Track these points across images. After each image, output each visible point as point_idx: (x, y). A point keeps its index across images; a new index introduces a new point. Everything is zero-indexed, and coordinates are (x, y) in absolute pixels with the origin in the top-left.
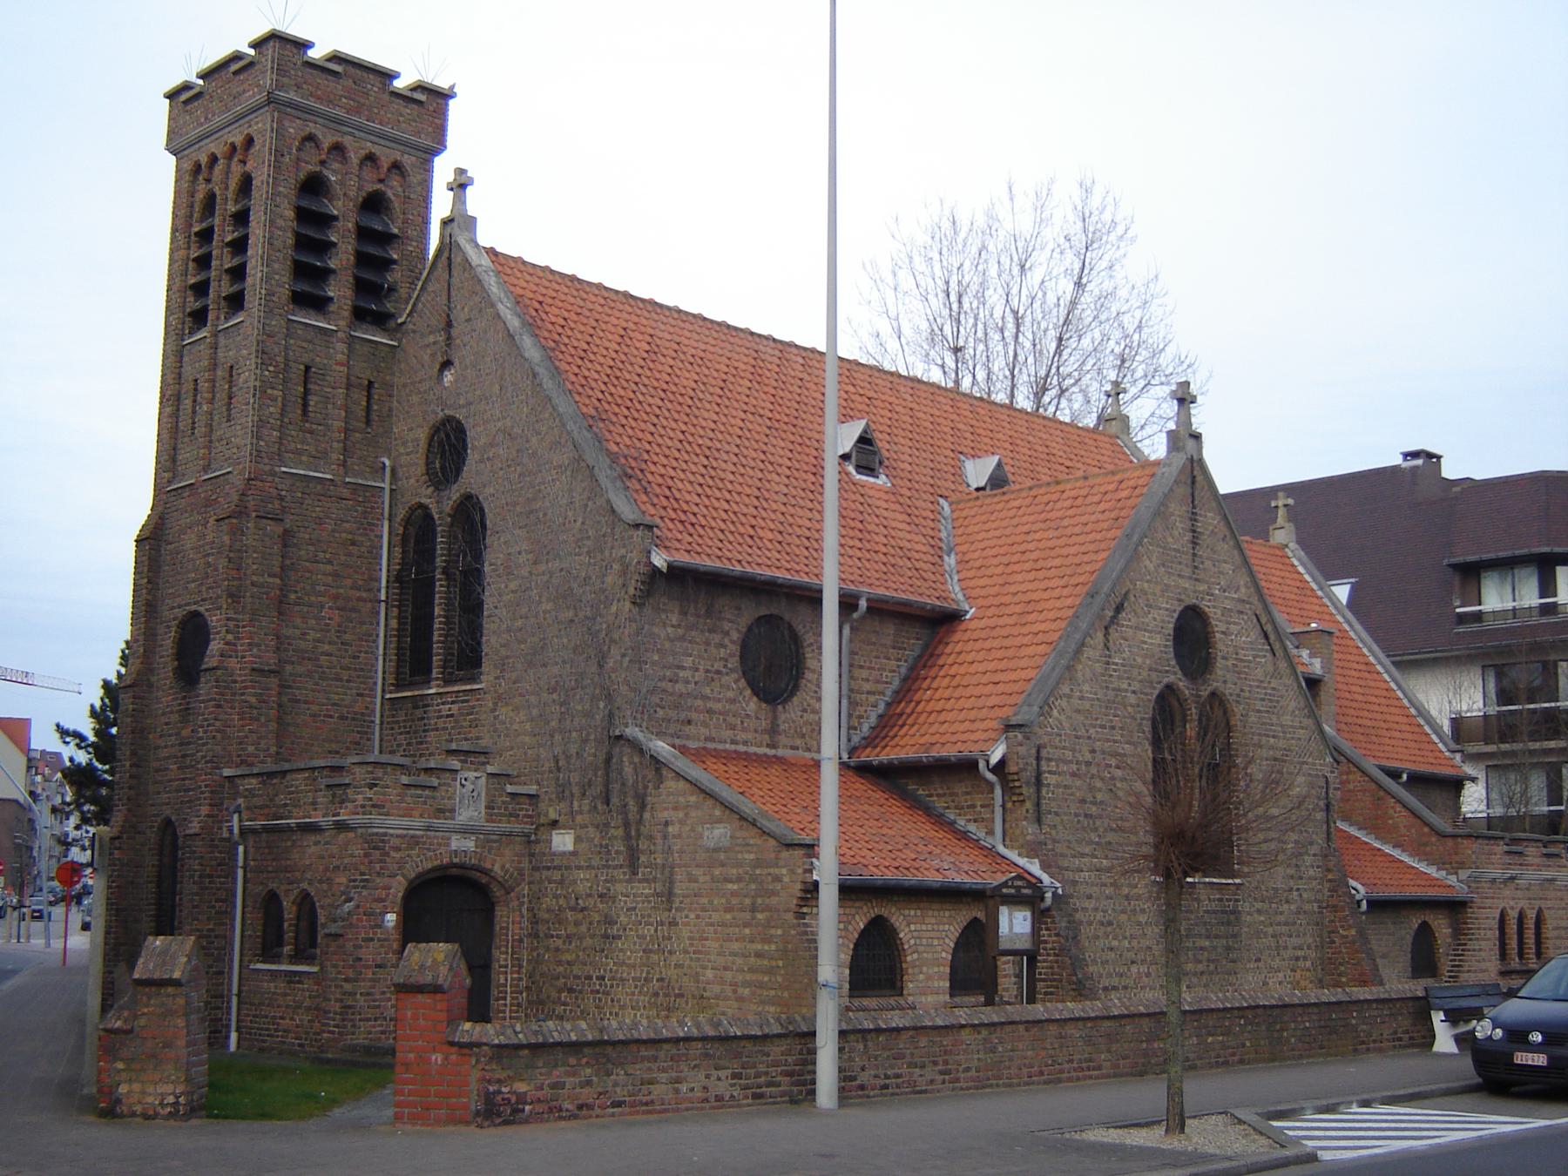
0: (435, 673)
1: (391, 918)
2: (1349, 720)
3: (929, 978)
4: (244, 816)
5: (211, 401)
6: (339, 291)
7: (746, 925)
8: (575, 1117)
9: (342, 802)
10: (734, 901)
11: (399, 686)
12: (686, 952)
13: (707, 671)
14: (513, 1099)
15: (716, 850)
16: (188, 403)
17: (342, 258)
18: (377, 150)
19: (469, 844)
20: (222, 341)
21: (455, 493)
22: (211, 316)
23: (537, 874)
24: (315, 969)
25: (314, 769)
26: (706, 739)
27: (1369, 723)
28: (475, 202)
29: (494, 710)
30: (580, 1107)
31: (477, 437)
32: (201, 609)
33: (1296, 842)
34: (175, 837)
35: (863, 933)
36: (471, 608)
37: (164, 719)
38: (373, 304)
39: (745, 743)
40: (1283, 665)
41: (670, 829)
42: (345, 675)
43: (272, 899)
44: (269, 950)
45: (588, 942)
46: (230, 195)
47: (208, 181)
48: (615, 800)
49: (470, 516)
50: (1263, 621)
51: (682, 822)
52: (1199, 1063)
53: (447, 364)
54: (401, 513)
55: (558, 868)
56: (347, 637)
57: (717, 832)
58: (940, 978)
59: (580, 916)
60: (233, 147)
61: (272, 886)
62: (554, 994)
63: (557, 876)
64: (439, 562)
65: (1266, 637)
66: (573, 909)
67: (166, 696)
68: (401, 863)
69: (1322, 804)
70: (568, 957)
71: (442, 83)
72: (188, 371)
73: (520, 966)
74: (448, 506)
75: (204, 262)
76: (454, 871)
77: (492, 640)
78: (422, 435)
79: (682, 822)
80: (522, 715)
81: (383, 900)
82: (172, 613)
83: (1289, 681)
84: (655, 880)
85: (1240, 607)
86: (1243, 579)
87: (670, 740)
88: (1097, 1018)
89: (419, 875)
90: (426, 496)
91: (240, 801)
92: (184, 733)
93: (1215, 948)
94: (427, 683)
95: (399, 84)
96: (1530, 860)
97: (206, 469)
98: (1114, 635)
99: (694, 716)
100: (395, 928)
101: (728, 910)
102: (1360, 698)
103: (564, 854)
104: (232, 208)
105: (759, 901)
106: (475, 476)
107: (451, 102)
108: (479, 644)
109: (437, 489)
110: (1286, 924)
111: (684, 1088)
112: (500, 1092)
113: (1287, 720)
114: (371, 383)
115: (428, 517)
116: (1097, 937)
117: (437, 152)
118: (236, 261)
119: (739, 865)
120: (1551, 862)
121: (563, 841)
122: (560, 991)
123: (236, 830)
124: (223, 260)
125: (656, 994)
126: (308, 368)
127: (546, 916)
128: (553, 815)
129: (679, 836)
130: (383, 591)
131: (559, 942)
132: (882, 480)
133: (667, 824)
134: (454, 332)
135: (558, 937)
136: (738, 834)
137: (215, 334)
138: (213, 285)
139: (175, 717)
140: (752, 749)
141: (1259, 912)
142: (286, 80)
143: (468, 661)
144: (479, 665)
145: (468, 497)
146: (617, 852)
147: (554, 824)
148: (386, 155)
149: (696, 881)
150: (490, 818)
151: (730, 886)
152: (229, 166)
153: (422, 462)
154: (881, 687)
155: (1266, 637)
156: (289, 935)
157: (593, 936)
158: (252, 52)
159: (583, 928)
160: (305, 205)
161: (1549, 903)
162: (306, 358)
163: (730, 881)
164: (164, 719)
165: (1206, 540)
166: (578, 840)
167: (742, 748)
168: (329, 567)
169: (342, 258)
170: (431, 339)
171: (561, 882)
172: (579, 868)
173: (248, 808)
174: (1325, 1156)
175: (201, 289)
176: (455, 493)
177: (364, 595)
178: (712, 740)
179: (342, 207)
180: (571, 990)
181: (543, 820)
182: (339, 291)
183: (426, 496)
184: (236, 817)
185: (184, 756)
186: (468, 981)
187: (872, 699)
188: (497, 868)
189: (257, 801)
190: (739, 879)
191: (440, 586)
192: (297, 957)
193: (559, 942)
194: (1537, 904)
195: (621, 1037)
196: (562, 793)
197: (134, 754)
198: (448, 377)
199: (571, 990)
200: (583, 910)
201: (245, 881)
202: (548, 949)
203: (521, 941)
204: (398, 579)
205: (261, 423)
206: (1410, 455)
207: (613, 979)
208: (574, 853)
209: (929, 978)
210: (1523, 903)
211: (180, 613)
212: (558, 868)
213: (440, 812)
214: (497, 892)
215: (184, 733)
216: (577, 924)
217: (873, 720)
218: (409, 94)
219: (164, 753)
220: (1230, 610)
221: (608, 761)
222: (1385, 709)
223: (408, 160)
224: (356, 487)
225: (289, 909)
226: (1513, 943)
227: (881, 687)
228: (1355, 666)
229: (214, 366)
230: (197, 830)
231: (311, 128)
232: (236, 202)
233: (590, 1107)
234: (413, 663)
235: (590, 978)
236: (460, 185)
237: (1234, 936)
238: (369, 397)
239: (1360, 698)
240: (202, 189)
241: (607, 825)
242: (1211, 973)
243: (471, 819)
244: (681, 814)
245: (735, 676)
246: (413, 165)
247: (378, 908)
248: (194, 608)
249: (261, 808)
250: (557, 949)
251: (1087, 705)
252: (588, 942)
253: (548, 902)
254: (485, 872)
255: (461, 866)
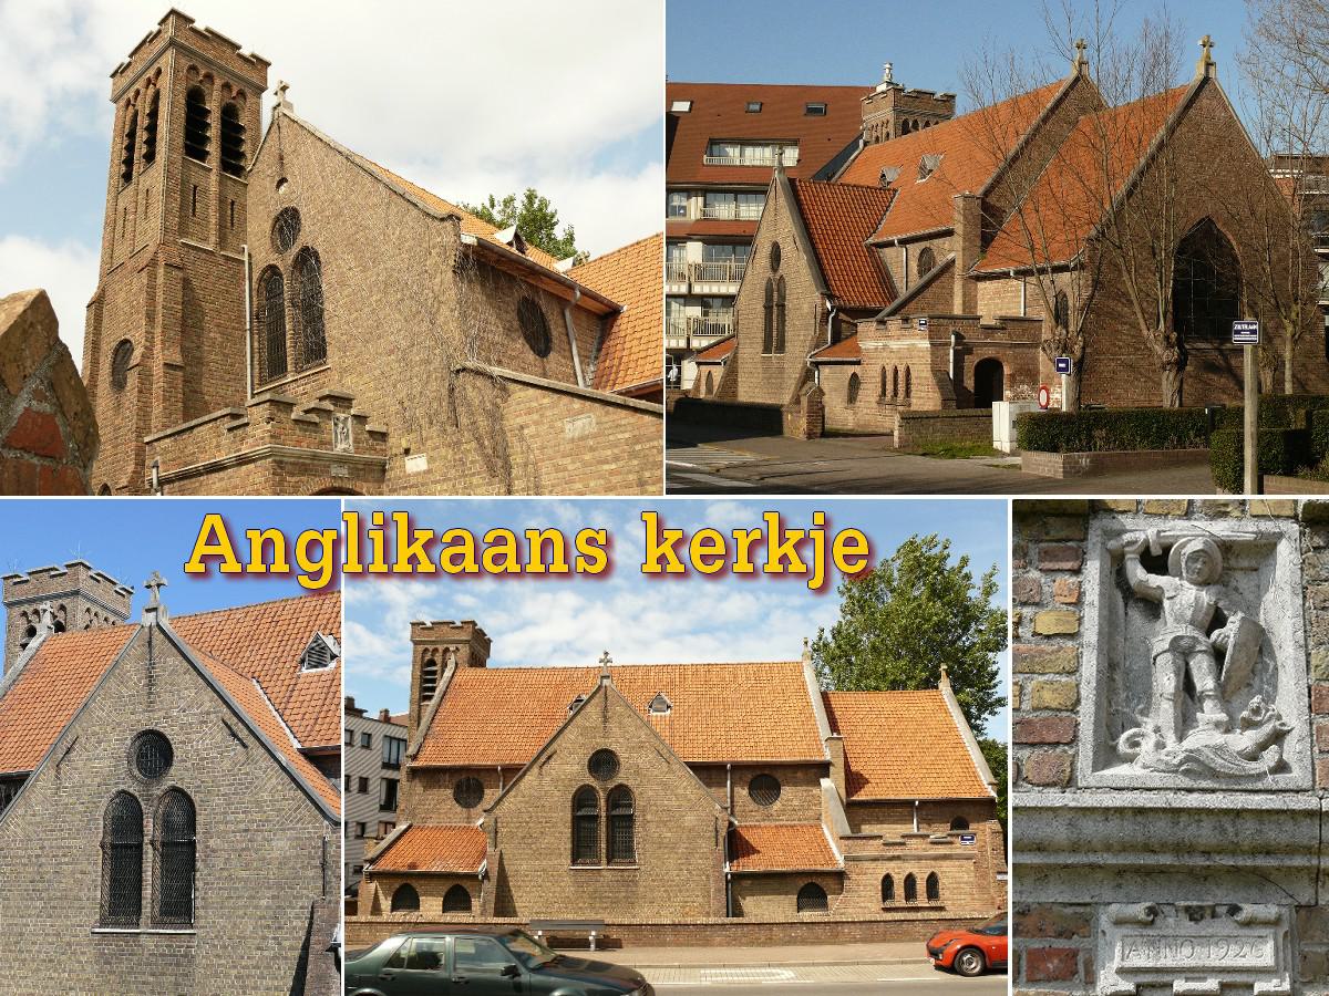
4: (160, 469)
6: (213, 148)
10: (614, 480)
15: (582, 438)
17: (214, 131)
18: (231, 82)
25: (215, 419)
38: (232, 161)
41: (526, 431)
47: (134, 105)
48: (464, 420)
53: (282, 181)
54: (256, 276)
57: (579, 423)
77: (333, 330)
78: (267, 226)
79: (536, 423)
80: (366, 378)
90: (274, 259)
103: (418, 474)
105: (647, 474)
106: (309, 234)
107: (269, 69)
123: (155, 481)
128: (405, 445)
129: (538, 435)
130: (248, 324)
133: (522, 428)
136: (605, 419)
145: (305, 249)
146: (472, 462)
149: (565, 470)
151: (606, 467)
153: (269, 241)
163: (606, 462)
166: (431, 460)
169: (214, 131)
173: (164, 462)
176: (295, 250)
179: (213, 105)
182: (213, 148)
184: (154, 470)
185: (117, 438)
190: (616, 459)
196: (410, 426)
198: (283, 189)
205: (167, 212)
208: (429, 471)
213: (322, 443)
221: (452, 390)
224: (227, 258)
230: (126, 484)
231: (23, 608)
243: (345, 450)
244: (535, 417)
249: (174, 460)
251: (38, 819)
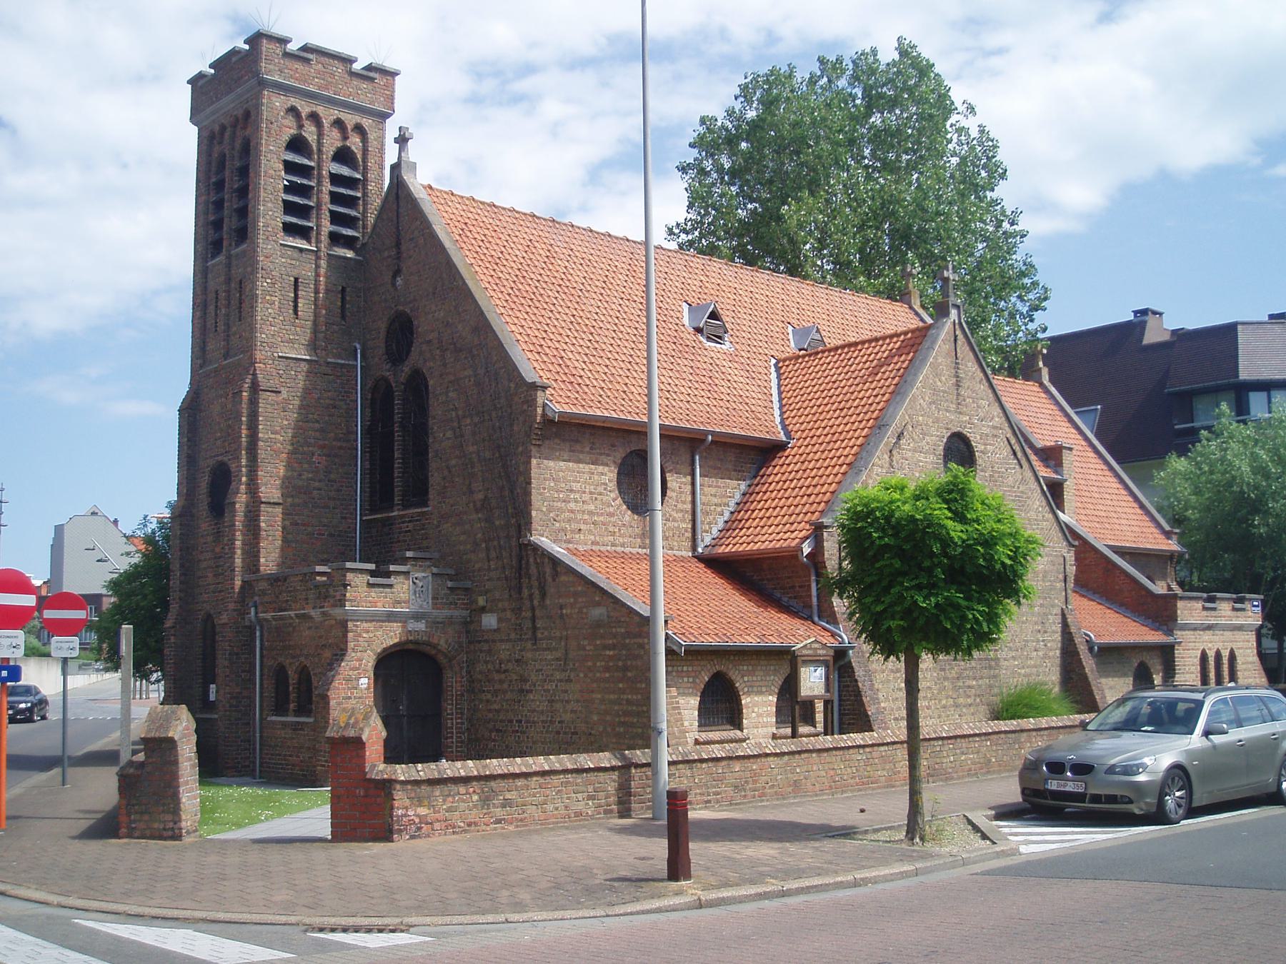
0: (397, 500)
1: (364, 682)
2: (1088, 512)
3: (759, 715)
5: (228, 306)
7: (620, 681)
8: (466, 831)
9: (326, 597)
11: (373, 511)
12: (578, 701)
13: (591, 493)
14: (417, 820)
16: (212, 308)
18: (343, 116)
19: (421, 626)
20: (234, 262)
21: (406, 369)
22: (225, 243)
23: (472, 647)
24: (311, 720)
26: (593, 543)
27: (1103, 514)
28: (414, 152)
29: (438, 526)
30: (469, 825)
31: (423, 326)
32: (226, 459)
33: (1041, 605)
34: (214, 626)
35: (708, 685)
36: (419, 451)
37: (202, 541)
39: (623, 545)
40: (1029, 474)
42: (331, 504)
43: (281, 673)
44: (280, 709)
45: (509, 695)
46: (236, 154)
49: (418, 385)
50: (1013, 441)
51: (572, 606)
52: (955, 775)
53: (397, 272)
55: (486, 641)
56: (332, 476)
58: (768, 715)
59: (503, 676)
60: (237, 120)
61: (281, 659)
62: (487, 734)
63: (486, 647)
64: (397, 418)
65: (1015, 453)
66: (498, 672)
67: (205, 526)
68: (369, 642)
69: (1061, 576)
70: (496, 706)
71: (390, 64)
72: (212, 285)
73: (462, 714)
74: (403, 377)
75: (219, 205)
76: (411, 647)
78: (383, 326)
81: (358, 669)
82: (206, 464)
83: (1034, 486)
84: (556, 649)
85: (995, 432)
86: (996, 410)
87: (564, 545)
88: (873, 745)
89: (385, 650)
90: (385, 371)
91: (256, 598)
92: (217, 550)
93: (980, 686)
94: (391, 508)
95: (357, 67)
96: (1223, 613)
97: (226, 356)
98: (896, 457)
99: (583, 527)
100: (368, 689)
101: (607, 669)
102: (1097, 495)
104: (238, 164)
108: (427, 478)
109: (394, 364)
110: (1035, 666)
111: (550, 807)
112: (406, 815)
113: (1032, 515)
114: (343, 290)
115: (389, 386)
116: (889, 681)
117: (389, 115)
118: (241, 204)
119: (615, 636)
120: (1239, 613)
121: (490, 621)
122: (491, 731)
124: (231, 204)
125: (558, 733)
126: (296, 280)
127: (480, 677)
131: (489, 696)
132: (726, 346)
134: (403, 248)
135: (488, 692)
137: (229, 257)
138: (226, 220)
139: (210, 539)
140: (627, 550)
141: (1014, 658)
142: (271, 67)
143: (418, 492)
144: (427, 492)
147: (483, 610)
148: (350, 119)
150: (435, 606)
152: (234, 133)
153: (383, 345)
154: (725, 500)
155: (1015, 453)
156: (293, 696)
157: (512, 691)
158: (247, 47)
159: (505, 686)
160: (278, 156)
161: (1240, 645)
162: (295, 273)
164: (202, 541)
165: (965, 383)
166: (500, 620)
167: (619, 549)
168: (317, 425)
170: (386, 254)
171: (489, 651)
172: (502, 641)
174: (1023, 849)
175: (218, 225)
176: (406, 369)
177: (344, 445)
178: (598, 544)
180: (498, 731)
181: (474, 607)
183: (385, 371)
186: (384, 734)
187: (719, 509)
188: (442, 642)
189: (266, 599)
191: (397, 436)
192: (298, 712)
193: (489, 696)
194: (1229, 645)
195: (500, 772)
197: (182, 566)
199: (498, 731)
200: (505, 671)
201: (262, 656)
202: (481, 701)
203: (462, 695)
204: (367, 432)
206: (1136, 312)
207: (527, 722)
209: (759, 715)
210: (1220, 645)
211: (211, 462)
212: (486, 641)
214: (442, 660)
215: (217, 550)
216: (501, 682)
217: (721, 525)
218: (365, 73)
219: (204, 565)
220: (987, 435)
222: (1115, 503)
223: (367, 122)
225: (293, 677)
226: (1212, 675)
227: (725, 500)
228: (1093, 472)
229: (228, 280)
232: (241, 158)
233: (476, 824)
234: (380, 496)
235: (511, 721)
236: (402, 140)
237: (995, 677)
238: (343, 299)
239: (1097, 495)
240: (217, 149)
241: (520, 609)
242: (978, 705)
245: (613, 495)
246: (370, 126)
247: (353, 674)
248: (220, 458)
250: (488, 701)
252: (509, 695)
253: (480, 667)
254: (434, 646)
255: (416, 642)
